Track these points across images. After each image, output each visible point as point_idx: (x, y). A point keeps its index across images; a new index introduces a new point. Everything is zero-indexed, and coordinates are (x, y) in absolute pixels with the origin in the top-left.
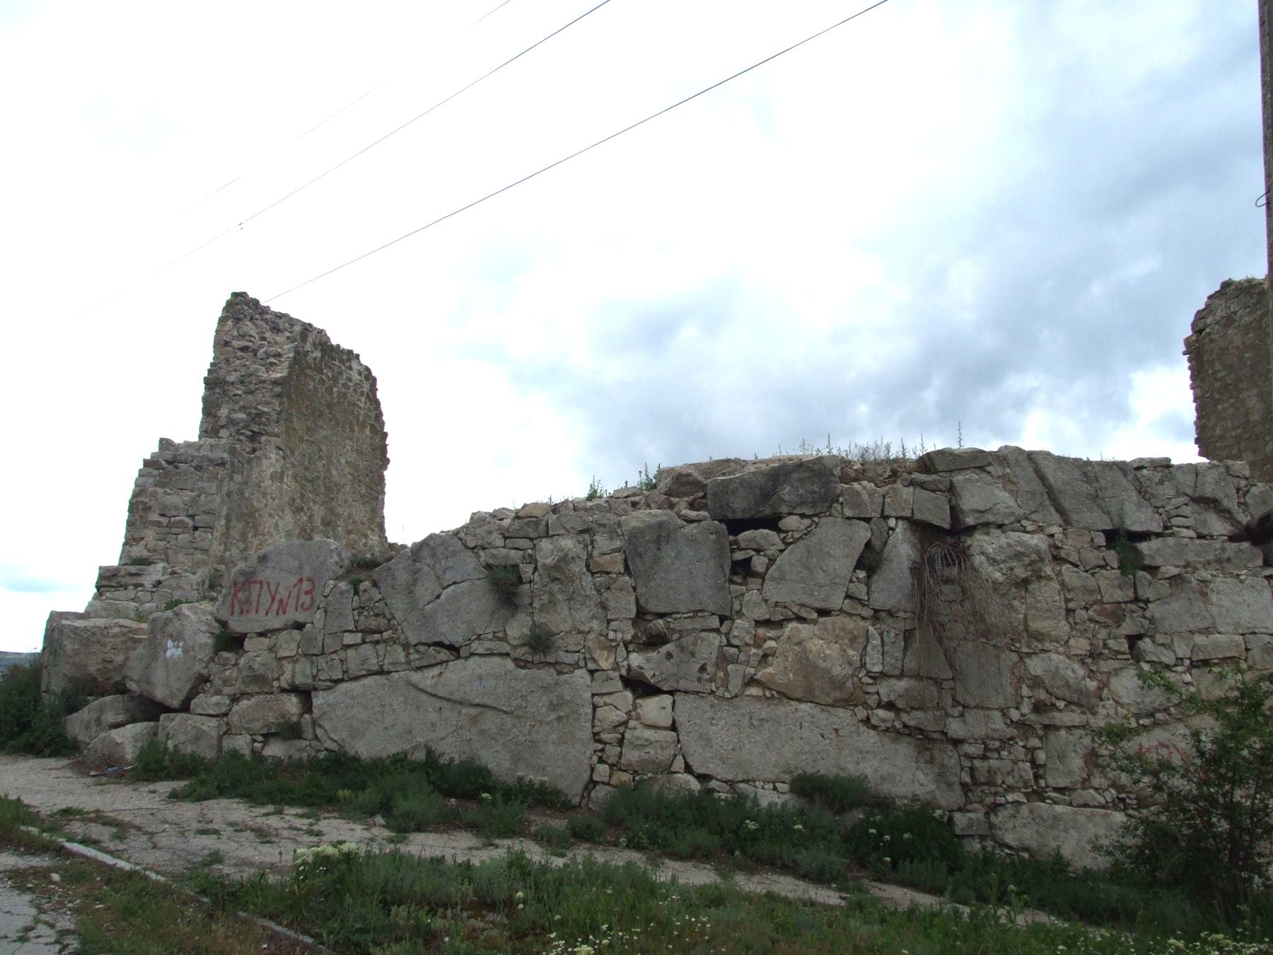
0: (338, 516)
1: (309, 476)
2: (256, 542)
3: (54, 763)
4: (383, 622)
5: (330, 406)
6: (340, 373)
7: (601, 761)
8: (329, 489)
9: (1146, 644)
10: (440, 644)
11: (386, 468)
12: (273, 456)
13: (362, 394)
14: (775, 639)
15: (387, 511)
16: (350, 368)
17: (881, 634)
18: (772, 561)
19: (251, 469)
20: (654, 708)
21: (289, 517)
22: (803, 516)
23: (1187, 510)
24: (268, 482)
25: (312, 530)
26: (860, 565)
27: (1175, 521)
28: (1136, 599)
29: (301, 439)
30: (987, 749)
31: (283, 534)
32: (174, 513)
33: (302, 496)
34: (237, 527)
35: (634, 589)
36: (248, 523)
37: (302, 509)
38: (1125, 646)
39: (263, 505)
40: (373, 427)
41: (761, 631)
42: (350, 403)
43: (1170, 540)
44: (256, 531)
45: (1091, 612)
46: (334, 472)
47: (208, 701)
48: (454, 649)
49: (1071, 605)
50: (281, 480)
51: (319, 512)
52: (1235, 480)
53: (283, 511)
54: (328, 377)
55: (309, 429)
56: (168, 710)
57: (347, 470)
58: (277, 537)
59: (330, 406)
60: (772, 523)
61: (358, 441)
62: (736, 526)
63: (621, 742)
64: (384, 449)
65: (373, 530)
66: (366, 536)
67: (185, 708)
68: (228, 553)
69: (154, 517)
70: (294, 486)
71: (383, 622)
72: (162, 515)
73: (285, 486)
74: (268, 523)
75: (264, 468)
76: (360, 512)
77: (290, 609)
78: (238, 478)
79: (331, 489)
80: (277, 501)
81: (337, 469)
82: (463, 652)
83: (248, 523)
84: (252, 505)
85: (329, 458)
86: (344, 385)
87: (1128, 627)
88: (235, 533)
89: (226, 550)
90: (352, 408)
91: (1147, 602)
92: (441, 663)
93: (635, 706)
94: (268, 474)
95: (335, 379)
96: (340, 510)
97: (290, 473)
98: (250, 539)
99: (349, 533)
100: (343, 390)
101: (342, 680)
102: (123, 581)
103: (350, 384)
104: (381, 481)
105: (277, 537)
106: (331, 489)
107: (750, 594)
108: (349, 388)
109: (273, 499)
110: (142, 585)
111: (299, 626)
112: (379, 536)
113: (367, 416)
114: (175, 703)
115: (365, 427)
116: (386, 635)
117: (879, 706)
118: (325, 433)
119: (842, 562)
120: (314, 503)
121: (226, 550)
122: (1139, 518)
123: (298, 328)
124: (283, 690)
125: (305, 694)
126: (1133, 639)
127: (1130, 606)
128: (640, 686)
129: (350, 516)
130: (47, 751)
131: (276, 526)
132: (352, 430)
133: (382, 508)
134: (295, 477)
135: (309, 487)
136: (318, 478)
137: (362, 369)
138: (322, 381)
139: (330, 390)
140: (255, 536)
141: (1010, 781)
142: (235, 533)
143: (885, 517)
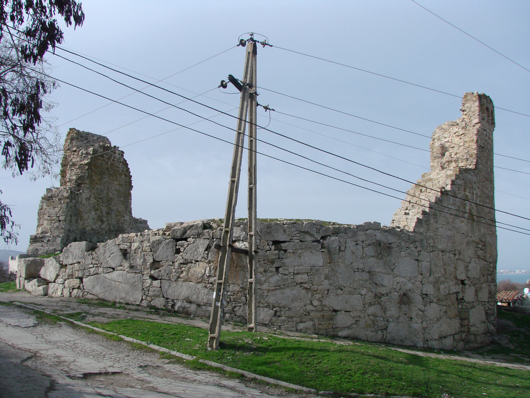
0: (112, 210)
1: (100, 197)
2: (81, 223)
3: (217, 379)
4: (98, 262)
5: (107, 169)
6: (111, 156)
7: (144, 294)
8: (108, 201)
9: (280, 269)
10: (110, 267)
11: (131, 190)
12: (86, 192)
13: (120, 162)
14: (185, 267)
15: (133, 206)
16: (115, 153)
17: (210, 267)
18: (185, 249)
19: (78, 197)
20: (156, 283)
21: (93, 213)
22: (193, 238)
23: (298, 235)
24: (84, 201)
25: (102, 217)
26: (206, 250)
27: (293, 238)
28: (279, 258)
29: (97, 184)
30: (234, 294)
31: (91, 219)
32: (52, 216)
33: (98, 204)
34: (74, 218)
35: (153, 255)
36: (78, 217)
37: (98, 209)
38: (274, 270)
39: (83, 210)
40: (125, 174)
41: (182, 266)
42: (115, 167)
43: (292, 243)
44: (81, 219)
45: (265, 262)
46: (110, 194)
47: (60, 280)
48: (114, 269)
49: (259, 260)
50: (89, 199)
51: (104, 209)
52: (316, 226)
53: (91, 211)
54: (106, 158)
55: (99, 179)
56: (51, 282)
57: (115, 192)
58: (89, 221)
59: (107, 169)
60: (186, 239)
61: (119, 181)
62: (177, 240)
63: (148, 290)
64: (130, 182)
65: (127, 214)
66: (124, 216)
67: (54, 282)
68: (71, 228)
69: (46, 217)
70: (95, 201)
71: (98, 262)
72: (49, 217)
73: (91, 202)
74: (86, 216)
75: (83, 196)
76: (121, 208)
77: (77, 258)
78: (74, 201)
79: (109, 201)
80: (88, 208)
81: (111, 192)
82: (115, 270)
83: (78, 217)
84: (80, 210)
85: (108, 188)
86: (112, 160)
87: (276, 265)
88: (74, 221)
89: (71, 227)
90: (116, 168)
91: (282, 259)
92: (111, 272)
93: (152, 282)
94: (85, 198)
95: (109, 158)
96: (113, 208)
97: (93, 197)
98: (79, 222)
99: (117, 216)
100: (112, 162)
101: (89, 276)
102: (38, 240)
103: (115, 159)
104: (130, 195)
105: (89, 221)
106: (109, 201)
107: (179, 256)
108: (115, 161)
109: (87, 207)
110: (43, 241)
111: (79, 263)
112: (130, 216)
113: (123, 170)
114: (53, 280)
115: (122, 175)
116: (99, 265)
117: (209, 283)
118: (105, 180)
119: (202, 249)
120: (103, 206)
121: (71, 227)
122: (281, 237)
123: (95, 138)
124: (76, 278)
125: (81, 279)
126: (277, 268)
127: (277, 260)
128: (153, 278)
129: (117, 210)
130: (95, 138)
131: (89, 216)
132: (117, 177)
133: (131, 205)
134: (95, 198)
135: (101, 201)
136: (104, 197)
137: (120, 153)
138: (104, 160)
139: (107, 163)
140: (81, 221)
141: (239, 301)
142: (74, 221)
143: (213, 238)
